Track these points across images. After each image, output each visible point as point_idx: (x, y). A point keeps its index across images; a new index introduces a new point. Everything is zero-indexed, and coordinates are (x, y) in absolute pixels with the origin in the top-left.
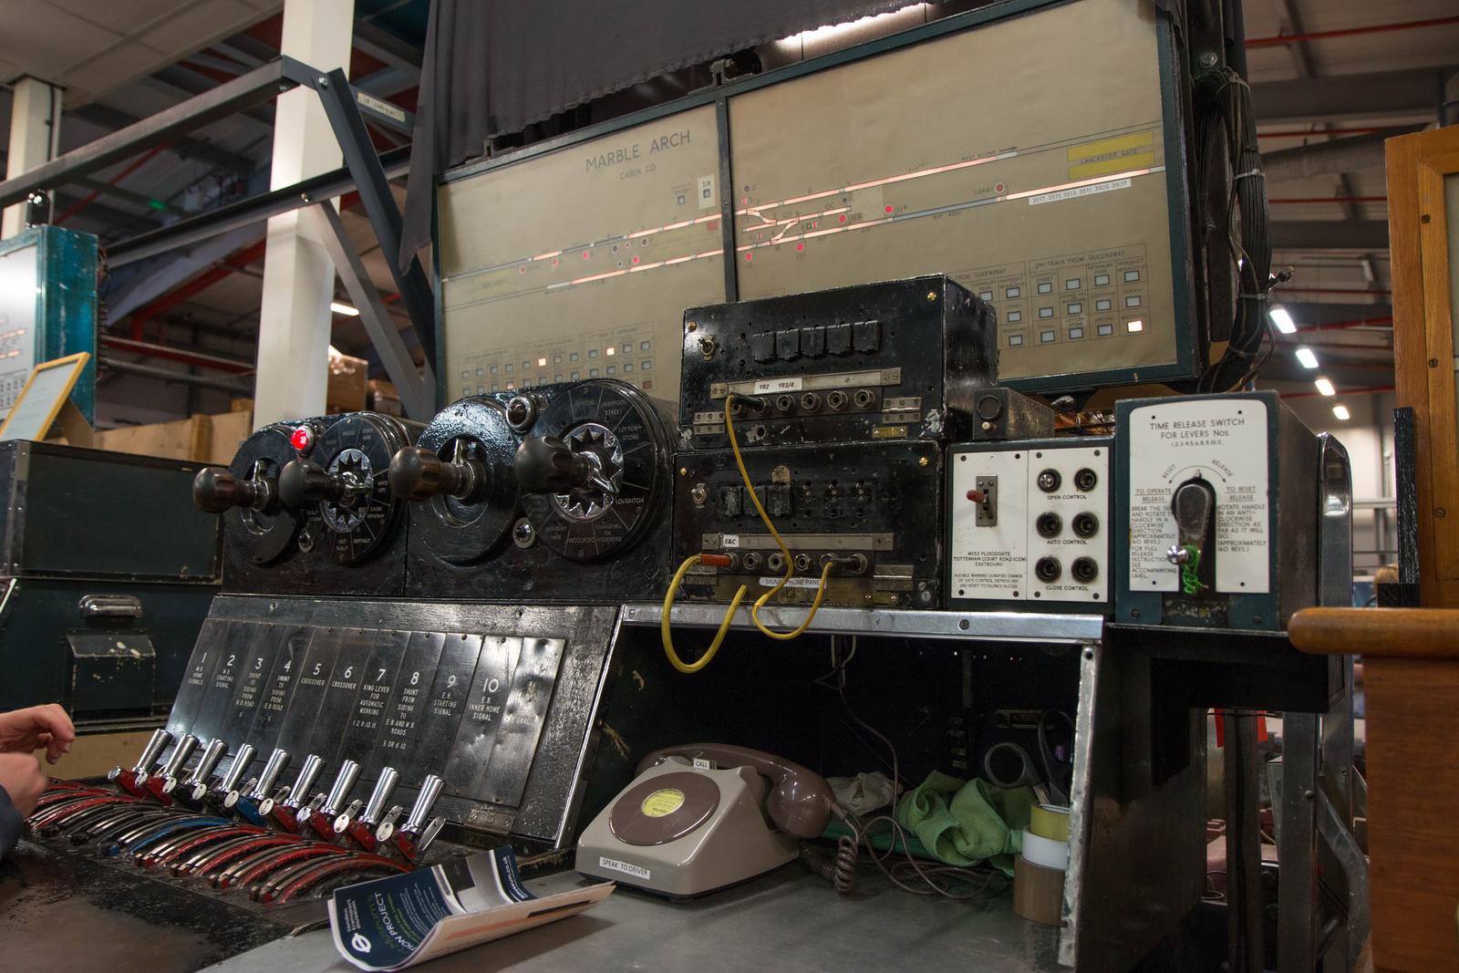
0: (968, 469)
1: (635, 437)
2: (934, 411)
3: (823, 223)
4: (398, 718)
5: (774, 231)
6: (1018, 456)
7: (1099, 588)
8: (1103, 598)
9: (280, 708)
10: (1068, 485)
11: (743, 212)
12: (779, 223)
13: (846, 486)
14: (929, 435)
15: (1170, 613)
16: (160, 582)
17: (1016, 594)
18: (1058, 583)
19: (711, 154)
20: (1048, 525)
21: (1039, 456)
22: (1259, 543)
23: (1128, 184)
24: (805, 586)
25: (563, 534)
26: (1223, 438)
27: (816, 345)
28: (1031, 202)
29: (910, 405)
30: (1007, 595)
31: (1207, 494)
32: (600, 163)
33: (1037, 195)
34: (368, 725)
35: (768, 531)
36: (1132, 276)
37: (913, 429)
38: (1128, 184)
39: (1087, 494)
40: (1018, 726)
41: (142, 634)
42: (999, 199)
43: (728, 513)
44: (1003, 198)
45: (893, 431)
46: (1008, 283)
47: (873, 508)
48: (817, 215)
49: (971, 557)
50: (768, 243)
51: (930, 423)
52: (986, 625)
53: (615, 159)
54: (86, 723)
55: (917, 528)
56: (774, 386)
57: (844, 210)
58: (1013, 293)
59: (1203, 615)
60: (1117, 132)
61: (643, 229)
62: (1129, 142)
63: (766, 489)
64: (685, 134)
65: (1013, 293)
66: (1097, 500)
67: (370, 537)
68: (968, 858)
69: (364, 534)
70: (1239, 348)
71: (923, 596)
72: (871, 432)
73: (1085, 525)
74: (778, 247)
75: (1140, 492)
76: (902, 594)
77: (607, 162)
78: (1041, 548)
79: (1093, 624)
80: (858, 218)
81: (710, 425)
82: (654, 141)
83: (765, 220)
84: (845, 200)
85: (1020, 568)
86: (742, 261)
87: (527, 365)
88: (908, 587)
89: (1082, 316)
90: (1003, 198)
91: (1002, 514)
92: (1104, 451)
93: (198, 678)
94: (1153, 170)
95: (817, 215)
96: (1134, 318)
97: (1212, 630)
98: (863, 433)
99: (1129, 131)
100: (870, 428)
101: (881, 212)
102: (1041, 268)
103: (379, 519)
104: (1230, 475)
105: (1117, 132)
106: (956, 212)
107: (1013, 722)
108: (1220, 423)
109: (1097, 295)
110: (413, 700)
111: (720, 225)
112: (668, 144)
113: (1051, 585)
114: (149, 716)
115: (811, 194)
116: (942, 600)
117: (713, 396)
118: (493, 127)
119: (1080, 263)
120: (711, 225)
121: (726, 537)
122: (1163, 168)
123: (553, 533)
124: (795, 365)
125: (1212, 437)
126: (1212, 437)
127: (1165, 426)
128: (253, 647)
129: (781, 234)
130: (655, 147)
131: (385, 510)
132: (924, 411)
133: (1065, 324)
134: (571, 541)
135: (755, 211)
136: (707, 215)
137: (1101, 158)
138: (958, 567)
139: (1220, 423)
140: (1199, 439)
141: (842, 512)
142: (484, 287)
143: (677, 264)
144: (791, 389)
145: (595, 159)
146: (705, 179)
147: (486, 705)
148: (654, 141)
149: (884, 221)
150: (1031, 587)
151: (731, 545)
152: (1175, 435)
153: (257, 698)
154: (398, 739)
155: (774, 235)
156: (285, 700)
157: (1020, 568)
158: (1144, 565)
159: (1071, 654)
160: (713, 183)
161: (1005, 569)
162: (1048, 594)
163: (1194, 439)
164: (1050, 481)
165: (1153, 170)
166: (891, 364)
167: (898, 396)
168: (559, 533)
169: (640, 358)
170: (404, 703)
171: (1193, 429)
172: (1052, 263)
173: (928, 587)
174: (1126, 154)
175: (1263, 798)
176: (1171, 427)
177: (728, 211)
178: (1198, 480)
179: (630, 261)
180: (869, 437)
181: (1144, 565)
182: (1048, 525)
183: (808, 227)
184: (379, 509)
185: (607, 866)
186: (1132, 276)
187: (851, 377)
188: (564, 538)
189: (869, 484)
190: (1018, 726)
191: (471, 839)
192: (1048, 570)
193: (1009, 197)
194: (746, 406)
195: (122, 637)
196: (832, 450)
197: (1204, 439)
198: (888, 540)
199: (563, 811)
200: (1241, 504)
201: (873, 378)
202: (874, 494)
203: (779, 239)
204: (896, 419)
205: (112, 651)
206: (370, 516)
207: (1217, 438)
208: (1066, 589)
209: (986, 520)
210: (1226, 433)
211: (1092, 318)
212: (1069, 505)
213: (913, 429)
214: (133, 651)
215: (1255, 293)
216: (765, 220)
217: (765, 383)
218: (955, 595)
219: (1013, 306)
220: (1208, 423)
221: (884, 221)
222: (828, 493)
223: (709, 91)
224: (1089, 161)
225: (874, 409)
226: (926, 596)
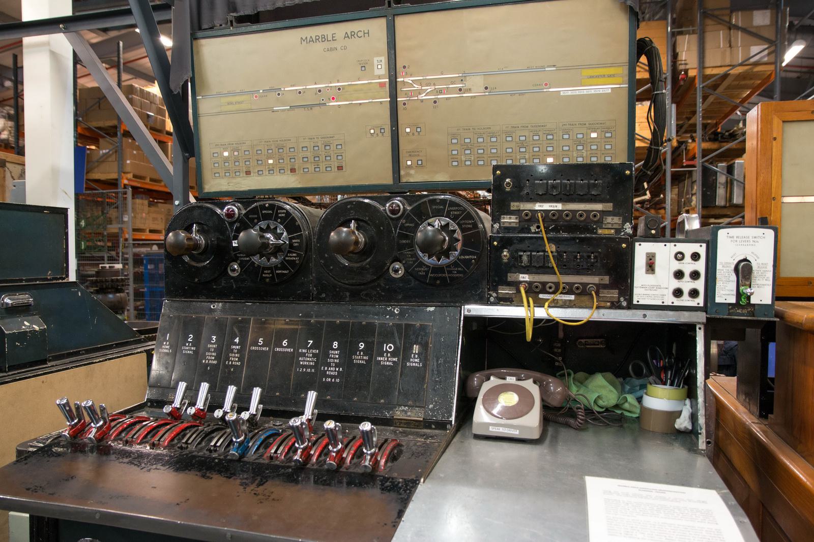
0: (642, 250)
1: (470, 226)
2: (628, 224)
3: (448, 91)
4: (329, 365)
5: (420, 92)
6: (665, 245)
7: (700, 301)
8: (702, 305)
9: (239, 364)
10: (688, 258)
11: (402, 79)
12: (423, 88)
13: (585, 254)
14: (626, 234)
15: (731, 311)
16: (38, 282)
17: (663, 303)
18: (682, 298)
19: (383, 45)
20: (679, 275)
21: (675, 245)
22: (768, 285)
23: (610, 91)
24: (563, 298)
25: (427, 272)
26: (756, 244)
27: (570, 189)
28: (562, 93)
29: (616, 220)
30: (659, 303)
31: (742, 264)
32: (310, 41)
33: (567, 91)
34: (309, 370)
35: (555, 274)
36: (608, 135)
37: (618, 231)
38: (610, 91)
39: (696, 262)
40: (588, 346)
41: (35, 315)
42: (545, 90)
43: (523, 264)
44: (547, 90)
45: (607, 232)
46: (548, 132)
47: (599, 265)
48: (445, 86)
49: (642, 286)
50: (416, 98)
51: (626, 229)
52: (653, 317)
53: (320, 40)
54: (16, 372)
55: (620, 274)
56: (546, 206)
57: (461, 85)
58: (550, 137)
59: (744, 312)
60: (606, 65)
61: (338, 81)
62: (612, 71)
63: (531, 254)
64: (366, 31)
65: (550, 137)
66: (700, 266)
67: (289, 269)
68: (602, 408)
69: (284, 267)
70: (647, 170)
71: (623, 303)
72: (597, 231)
73: (695, 275)
74: (422, 101)
75: (721, 263)
76: (612, 303)
77: (315, 41)
78: (676, 284)
79: (701, 317)
80: (469, 90)
81: (510, 223)
82: (346, 33)
83: (414, 85)
84: (462, 80)
85: (665, 292)
86: (400, 106)
87: (259, 152)
88: (616, 300)
89: (583, 151)
90: (547, 90)
91: (657, 269)
92: (704, 245)
93: (166, 349)
94: (622, 86)
95: (445, 86)
96: (550, 156)
97: (749, 318)
98: (592, 231)
99: (612, 65)
100: (596, 229)
101: (483, 89)
102: (564, 126)
103: (296, 260)
104: (758, 258)
105: (606, 65)
106: (520, 94)
107: (586, 345)
108: (755, 237)
109: (591, 142)
110: (337, 356)
111: (387, 85)
112: (355, 36)
113: (679, 299)
114: (47, 364)
115: (442, 74)
116: (631, 306)
117: (512, 209)
118: (232, 8)
119: (584, 126)
120: (382, 85)
121: (521, 275)
122: (627, 86)
123: (420, 271)
124: (544, 197)
125: (751, 243)
126: (751, 243)
127: (733, 237)
128: (205, 332)
129: (424, 94)
130: (347, 36)
131: (298, 255)
132: (623, 224)
133: (463, 159)
134: (432, 275)
135: (408, 80)
136: (380, 79)
137: (597, 77)
138: (636, 291)
139: (755, 237)
140: (747, 243)
141: (582, 266)
142: (228, 104)
143: (360, 104)
144: (555, 209)
145: (306, 38)
146: (379, 59)
147: (388, 358)
148: (346, 33)
149: (484, 94)
150: (670, 300)
151: (524, 279)
152: (736, 241)
153: (218, 358)
154: (331, 377)
155: (420, 94)
156: (240, 359)
157: (665, 292)
158: (722, 292)
159: (692, 327)
160: (383, 61)
161: (659, 292)
162: (678, 302)
163: (744, 243)
164: (679, 256)
165: (622, 86)
166: (607, 201)
167: (610, 216)
168: (423, 271)
169: (336, 153)
170: (331, 358)
171: (744, 239)
172: (570, 125)
173: (625, 300)
174: (610, 76)
175: (128, 308)
176: (735, 237)
177: (393, 78)
178: (745, 260)
179: (329, 99)
180: (596, 233)
181: (722, 292)
182: (679, 275)
183: (440, 92)
184: (294, 255)
185: (494, 430)
186: (608, 135)
187: (587, 205)
188: (427, 274)
189: (597, 254)
190: (588, 346)
191: (398, 424)
192: (678, 293)
193: (551, 90)
194: (532, 217)
195: (26, 318)
196: (578, 238)
197: (749, 243)
198: (606, 279)
199: (452, 407)
200: (762, 270)
201: (599, 207)
202: (599, 259)
203: (423, 96)
204: (610, 226)
205: (24, 327)
206: (287, 258)
207: (754, 243)
208: (686, 301)
209: (650, 271)
210: (758, 242)
211: (589, 153)
212: (688, 266)
213: (618, 231)
214: (34, 326)
215: (658, 146)
216: (414, 85)
217: (541, 204)
218: (635, 302)
219: (549, 144)
220: (751, 238)
221: (484, 94)
222: (576, 257)
223: (383, 9)
224: (592, 77)
225: (600, 223)
226: (624, 304)
